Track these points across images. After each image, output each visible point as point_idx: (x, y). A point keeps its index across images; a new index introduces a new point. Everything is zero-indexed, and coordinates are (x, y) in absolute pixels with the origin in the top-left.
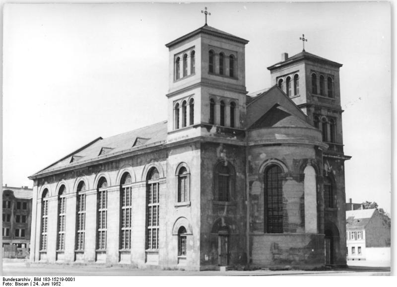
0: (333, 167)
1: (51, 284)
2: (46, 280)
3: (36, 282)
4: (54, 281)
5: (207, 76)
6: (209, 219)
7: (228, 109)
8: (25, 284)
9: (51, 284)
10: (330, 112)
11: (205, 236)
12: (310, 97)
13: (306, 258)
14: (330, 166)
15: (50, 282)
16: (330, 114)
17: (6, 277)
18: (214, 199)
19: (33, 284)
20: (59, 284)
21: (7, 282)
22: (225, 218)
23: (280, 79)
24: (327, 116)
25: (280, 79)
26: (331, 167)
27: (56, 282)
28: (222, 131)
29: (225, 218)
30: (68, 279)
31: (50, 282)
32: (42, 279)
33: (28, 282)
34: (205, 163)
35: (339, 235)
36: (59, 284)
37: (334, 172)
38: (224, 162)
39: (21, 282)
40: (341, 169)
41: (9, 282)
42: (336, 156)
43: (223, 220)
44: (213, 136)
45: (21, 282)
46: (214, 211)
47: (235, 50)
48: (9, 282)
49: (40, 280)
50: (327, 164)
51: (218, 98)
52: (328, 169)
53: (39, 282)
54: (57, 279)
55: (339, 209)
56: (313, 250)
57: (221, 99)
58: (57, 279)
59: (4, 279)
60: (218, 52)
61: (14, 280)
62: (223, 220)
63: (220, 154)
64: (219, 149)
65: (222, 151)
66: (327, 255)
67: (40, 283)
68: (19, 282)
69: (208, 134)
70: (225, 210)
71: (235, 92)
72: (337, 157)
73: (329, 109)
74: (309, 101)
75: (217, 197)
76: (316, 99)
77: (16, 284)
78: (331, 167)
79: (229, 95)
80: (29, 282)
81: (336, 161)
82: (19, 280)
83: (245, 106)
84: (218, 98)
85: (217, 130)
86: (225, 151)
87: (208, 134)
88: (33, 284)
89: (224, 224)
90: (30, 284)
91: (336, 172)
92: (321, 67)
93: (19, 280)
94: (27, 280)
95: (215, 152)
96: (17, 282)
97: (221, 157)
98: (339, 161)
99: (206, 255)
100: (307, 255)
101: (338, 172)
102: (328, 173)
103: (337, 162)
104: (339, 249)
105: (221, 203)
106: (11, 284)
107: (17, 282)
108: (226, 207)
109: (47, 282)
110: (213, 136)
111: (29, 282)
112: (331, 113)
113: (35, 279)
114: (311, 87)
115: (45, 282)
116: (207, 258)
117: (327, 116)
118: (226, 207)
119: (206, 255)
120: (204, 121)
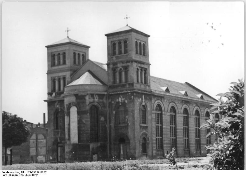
0: (125, 99)
1: (31, 175)
2: (29, 173)
3: (22, 174)
4: (33, 174)
5: (50, 68)
6: (52, 139)
7: (62, 82)
8: (16, 175)
9: (31, 175)
10: (124, 63)
11: (50, 148)
12: (110, 59)
13: (70, 157)
14: (123, 98)
15: (31, 174)
16: (124, 65)
17: (4, 171)
18: (54, 129)
19: (20, 175)
20: (36, 175)
21: (4, 174)
22: (60, 138)
23: (113, 42)
24: (122, 67)
25: (113, 42)
26: (124, 99)
27: (35, 174)
28: (58, 94)
29: (60, 138)
30: (42, 172)
31: (31, 174)
32: (26, 172)
33: (17, 174)
34: (50, 112)
35: (129, 141)
36: (36, 175)
37: (126, 101)
38: (59, 109)
39: (13, 174)
40: (131, 98)
41: (6, 174)
42: (123, 91)
43: (59, 139)
44: (53, 98)
45: (13, 174)
46: (54, 135)
47: (64, 49)
48: (6, 174)
49: (25, 172)
50: (121, 97)
51: (56, 78)
52: (122, 100)
53: (24, 174)
54: (35, 172)
55: (130, 124)
56: (74, 153)
57: (119, 42)
58: (35, 172)
59: (2, 172)
60: (56, 54)
61: (9, 172)
62: (59, 139)
63: (57, 106)
64: (56, 104)
65: (58, 105)
66: (123, 153)
67: (25, 174)
68: (12, 174)
69: (51, 97)
70: (60, 134)
71: (64, 72)
72: (124, 92)
73: (123, 62)
74: (109, 61)
75: (56, 128)
76: (114, 58)
77: (10, 175)
78: (124, 99)
79: (61, 74)
80: (18, 174)
81: (128, 94)
82: (12, 173)
83: (70, 77)
84: (56, 78)
85: (56, 94)
86: (59, 104)
87: (51, 97)
88: (20, 175)
89: (59, 141)
90: (18, 175)
91: (128, 101)
92: (118, 37)
93: (12, 173)
94: (16, 173)
95: (55, 105)
96: (11, 174)
97: (57, 107)
98: (130, 93)
99: (241, 151)
100: (71, 155)
101: (129, 100)
102: (121, 103)
103: (129, 95)
104: (130, 149)
105: (57, 130)
106: (7, 175)
107: (11, 174)
108: (60, 132)
109: (29, 174)
110: (53, 98)
111: (18, 174)
112: (125, 63)
113: (22, 172)
114: (111, 52)
115: (28, 174)
116: (100, 156)
117: (122, 67)
118: (60, 132)
119: (51, 157)
120: (49, 92)
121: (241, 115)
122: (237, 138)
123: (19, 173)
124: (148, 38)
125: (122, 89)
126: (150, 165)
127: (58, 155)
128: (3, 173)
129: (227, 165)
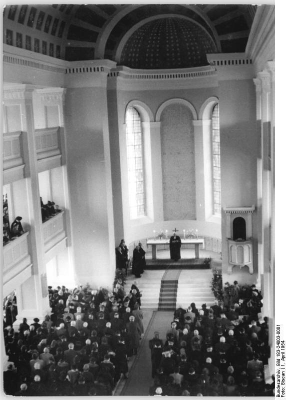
21: (281, 393)
30: (278, 332)
33: (281, 372)
41: (281, 390)
48: (281, 390)
59: (278, 396)
61: (279, 386)
68: (281, 380)
82: (279, 380)
93: (279, 380)
96: (280, 383)
107: (280, 383)
121: (240, 264)
122: (215, 378)
123: (280, 369)
124: (147, 260)
125: (137, 330)
126: (250, 250)
127: (6, 332)
128: (280, 395)
129: (221, 353)
